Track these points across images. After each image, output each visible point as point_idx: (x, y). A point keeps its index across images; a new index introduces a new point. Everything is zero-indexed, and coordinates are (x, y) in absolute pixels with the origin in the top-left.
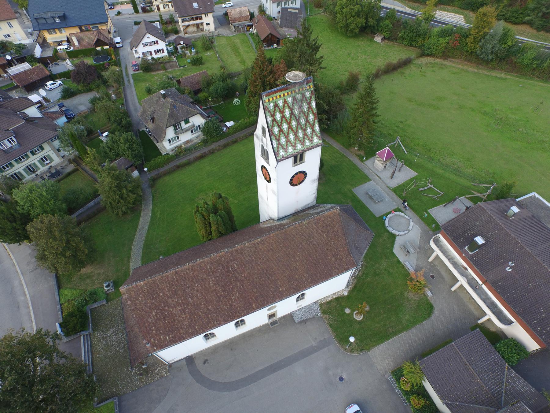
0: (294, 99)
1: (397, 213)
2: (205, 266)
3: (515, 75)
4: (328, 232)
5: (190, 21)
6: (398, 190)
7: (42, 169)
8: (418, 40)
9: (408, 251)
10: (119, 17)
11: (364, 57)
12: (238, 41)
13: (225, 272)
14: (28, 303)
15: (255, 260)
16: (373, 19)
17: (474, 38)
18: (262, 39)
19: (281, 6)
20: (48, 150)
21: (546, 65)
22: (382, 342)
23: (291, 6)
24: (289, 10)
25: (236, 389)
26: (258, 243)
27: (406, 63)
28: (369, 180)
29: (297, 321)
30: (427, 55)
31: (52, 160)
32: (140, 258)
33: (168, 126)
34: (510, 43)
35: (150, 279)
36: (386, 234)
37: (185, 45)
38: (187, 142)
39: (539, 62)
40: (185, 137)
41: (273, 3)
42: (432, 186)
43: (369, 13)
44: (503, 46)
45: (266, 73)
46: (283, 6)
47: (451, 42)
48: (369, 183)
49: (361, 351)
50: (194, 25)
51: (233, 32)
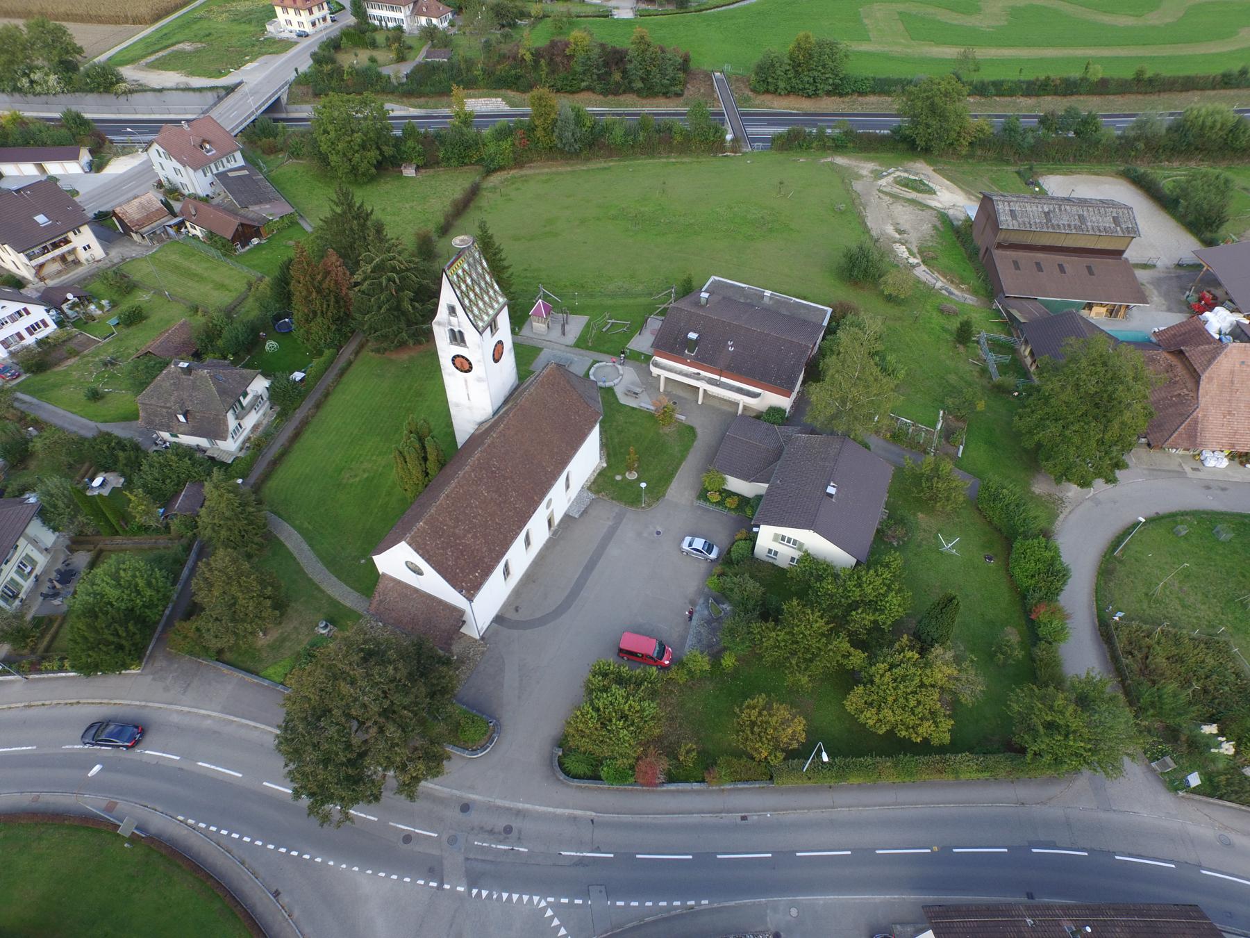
0: (469, 265)
1: (597, 365)
2: (470, 476)
3: (617, 159)
6: (581, 343)
8: (470, 154)
9: (635, 393)
11: (407, 206)
12: (175, 258)
14: (224, 720)
16: (388, 146)
17: (545, 130)
18: (230, 238)
19: (212, 172)
21: (641, 139)
23: (229, 166)
24: (230, 174)
25: (570, 607)
27: (474, 193)
28: (541, 349)
29: (577, 516)
30: (495, 170)
32: (335, 579)
34: (588, 124)
35: (427, 516)
37: (76, 299)
38: (255, 427)
39: (632, 137)
40: (251, 420)
41: (195, 170)
42: (613, 321)
43: (379, 138)
44: (584, 129)
45: (319, 277)
46: (215, 172)
47: (517, 142)
48: (543, 352)
49: (658, 500)
50: (53, 259)
51: (148, 246)
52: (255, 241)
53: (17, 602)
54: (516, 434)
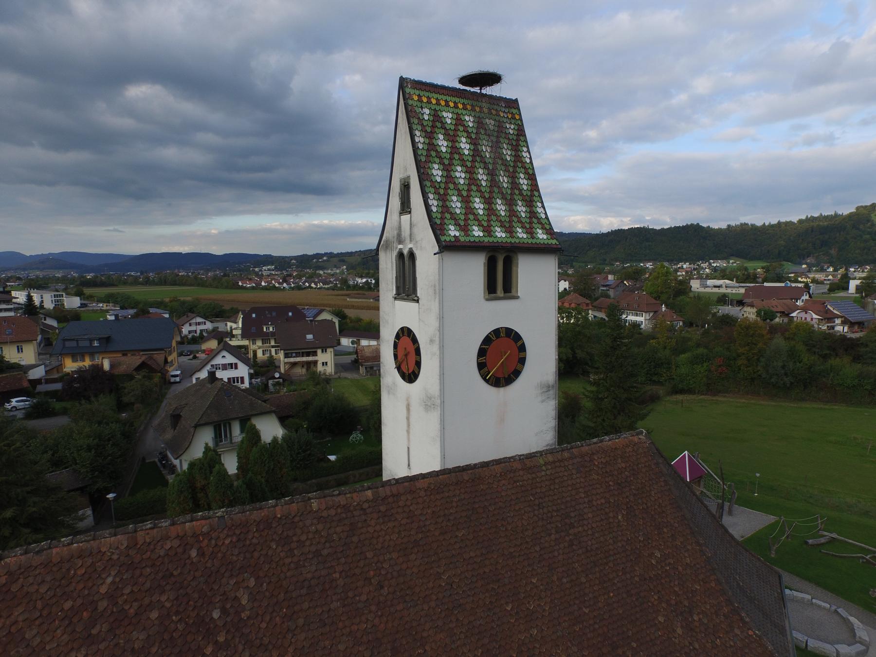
0: (480, 123)
5: (296, 356)
13: (180, 627)
15: (341, 582)
26: (366, 506)
33: (202, 422)
37: (281, 380)
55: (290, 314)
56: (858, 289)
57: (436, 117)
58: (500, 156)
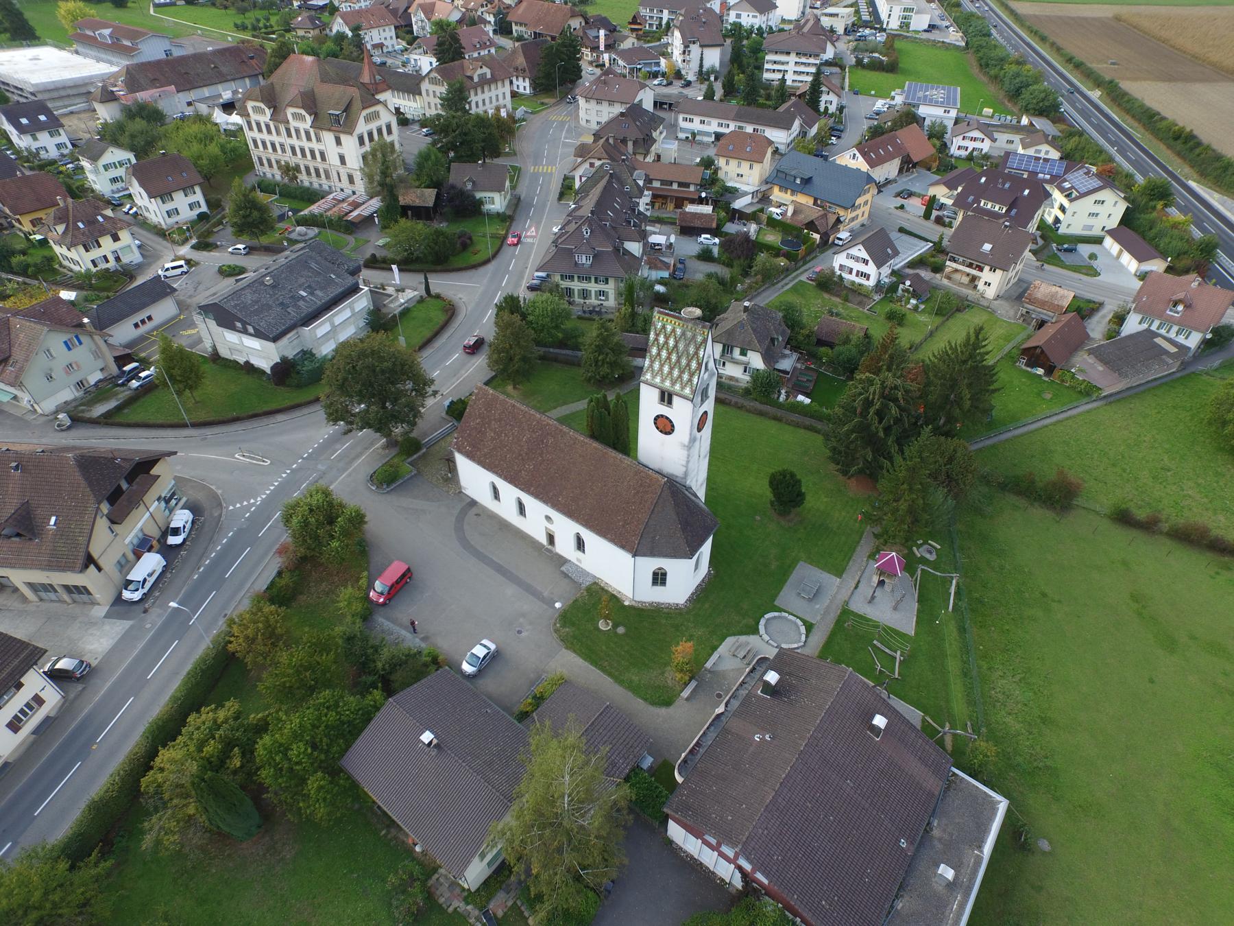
0: (683, 334)
1: (803, 629)
4: (638, 492)
7: (593, 301)
10: (899, 212)
20: (610, 288)
22: (585, 660)
24: (1158, 340)
31: (607, 299)
36: (752, 622)
38: (731, 378)
46: (1154, 328)
52: (1040, 371)
53: (582, 301)
54: (580, 456)
55: (1026, 192)
56: (798, 495)
57: (664, 327)
58: (687, 351)
